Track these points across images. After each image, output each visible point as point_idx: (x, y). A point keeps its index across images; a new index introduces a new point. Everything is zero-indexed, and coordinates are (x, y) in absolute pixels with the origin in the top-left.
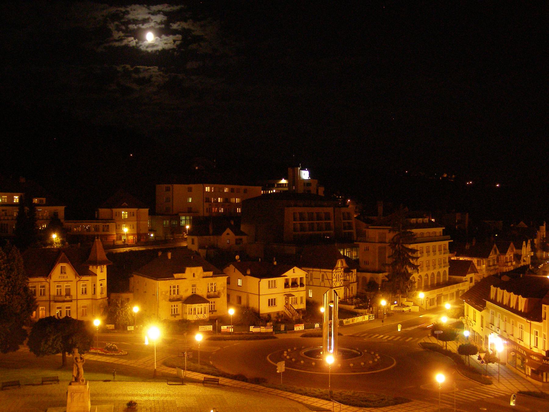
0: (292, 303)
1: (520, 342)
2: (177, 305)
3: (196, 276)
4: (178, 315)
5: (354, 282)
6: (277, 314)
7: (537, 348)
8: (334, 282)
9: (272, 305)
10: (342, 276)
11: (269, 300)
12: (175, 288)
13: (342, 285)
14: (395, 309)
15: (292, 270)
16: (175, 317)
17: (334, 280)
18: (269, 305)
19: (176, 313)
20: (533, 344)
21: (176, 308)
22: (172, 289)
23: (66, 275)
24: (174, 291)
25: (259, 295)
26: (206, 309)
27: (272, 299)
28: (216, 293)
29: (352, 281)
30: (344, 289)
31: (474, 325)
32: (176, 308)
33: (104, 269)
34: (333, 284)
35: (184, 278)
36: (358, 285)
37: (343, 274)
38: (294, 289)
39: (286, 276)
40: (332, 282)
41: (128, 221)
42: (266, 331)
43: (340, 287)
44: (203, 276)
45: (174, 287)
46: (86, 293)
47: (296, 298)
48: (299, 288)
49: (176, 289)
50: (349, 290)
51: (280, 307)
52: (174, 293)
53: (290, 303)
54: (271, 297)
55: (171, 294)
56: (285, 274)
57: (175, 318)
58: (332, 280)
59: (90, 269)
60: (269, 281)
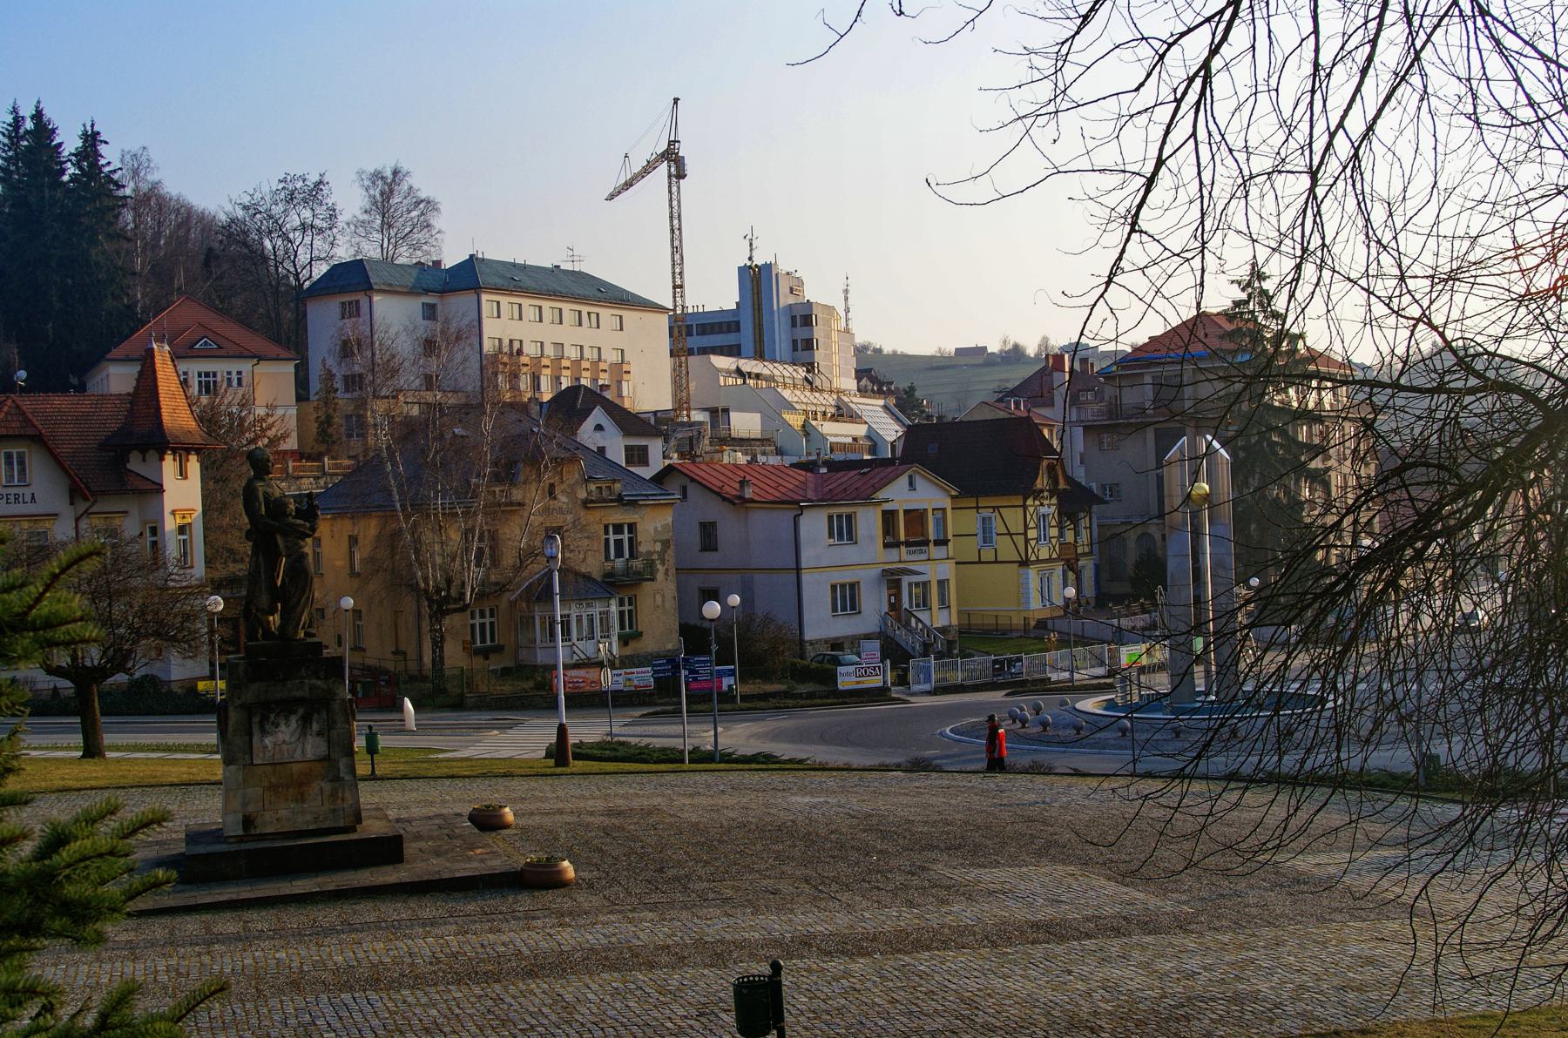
0: (911, 607)
2: (492, 611)
4: (499, 649)
8: (1033, 543)
9: (844, 609)
11: (834, 587)
12: (622, 533)
13: (1054, 556)
15: (904, 480)
16: (487, 658)
17: (1032, 534)
18: (834, 609)
19: (489, 643)
21: (487, 620)
22: (612, 537)
23: (27, 492)
24: (619, 543)
25: (798, 569)
26: (568, 622)
27: (843, 586)
28: (637, 564)
34: (1030, 550)
40: (1027, 541)
41: (1375, 384)
42: (858, 683)
43: (1050, 560)
45: (618, 529)
47: (926, 585)
48: (935, 552)
49: (626, 536)
52: (619, 554)
53: (906, 605)
54: (846, 577)
55: (607, 558)
56: (881, 495)
57: (487, 662)
58: (1025, 534)
59: (129, 466)
60: (830, 518)
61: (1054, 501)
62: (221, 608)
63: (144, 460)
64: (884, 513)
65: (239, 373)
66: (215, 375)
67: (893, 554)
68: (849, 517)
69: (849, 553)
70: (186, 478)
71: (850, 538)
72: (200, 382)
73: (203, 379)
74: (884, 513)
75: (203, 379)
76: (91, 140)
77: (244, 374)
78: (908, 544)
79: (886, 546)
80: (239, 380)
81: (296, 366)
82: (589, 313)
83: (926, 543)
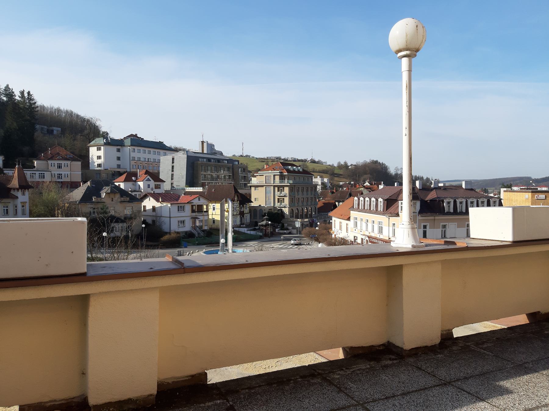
1: (380, 236)
3: (114, 200)
5: (247, 213)
6: (185, 233)
7: (395, 237)
10: (238, 207)
13: (238, 214)
14: (278, 232)
20: (391, 235)
29: (246, 212)
30: (240, 217)
31: (340, 233)
32: (60, 165)
33: (26, 192)
35: (103, 201)
36: (251, 215)
37: (239, 205)
38: (199, 214)
39: (193, 203)
44: (121, 201)
46: (7, 213)
50: (244, 218)
51: (188, 227)
54: (182, 219)
59: (11, 192)
60: (178, 207)
61: (238, 202)
62: (104, 233)
63: (14, 191)
64: (192, 205)
65: (67, 164)
66: (61, 164)
67: (194, 214)
68: (183, 207)
69: (182, 214)
70: (25, 195)
71: (183, 210)
72: (58, 166)
73: (58, 165)
74: (192, 205)
75: (58, 165)
76: (12, 89)
77: (55, 164)
78: (198, 212)
79: (192, 212)
80: (67, 166)
81: (81, 163)
82: (158, 152)
83: (202, 212)
